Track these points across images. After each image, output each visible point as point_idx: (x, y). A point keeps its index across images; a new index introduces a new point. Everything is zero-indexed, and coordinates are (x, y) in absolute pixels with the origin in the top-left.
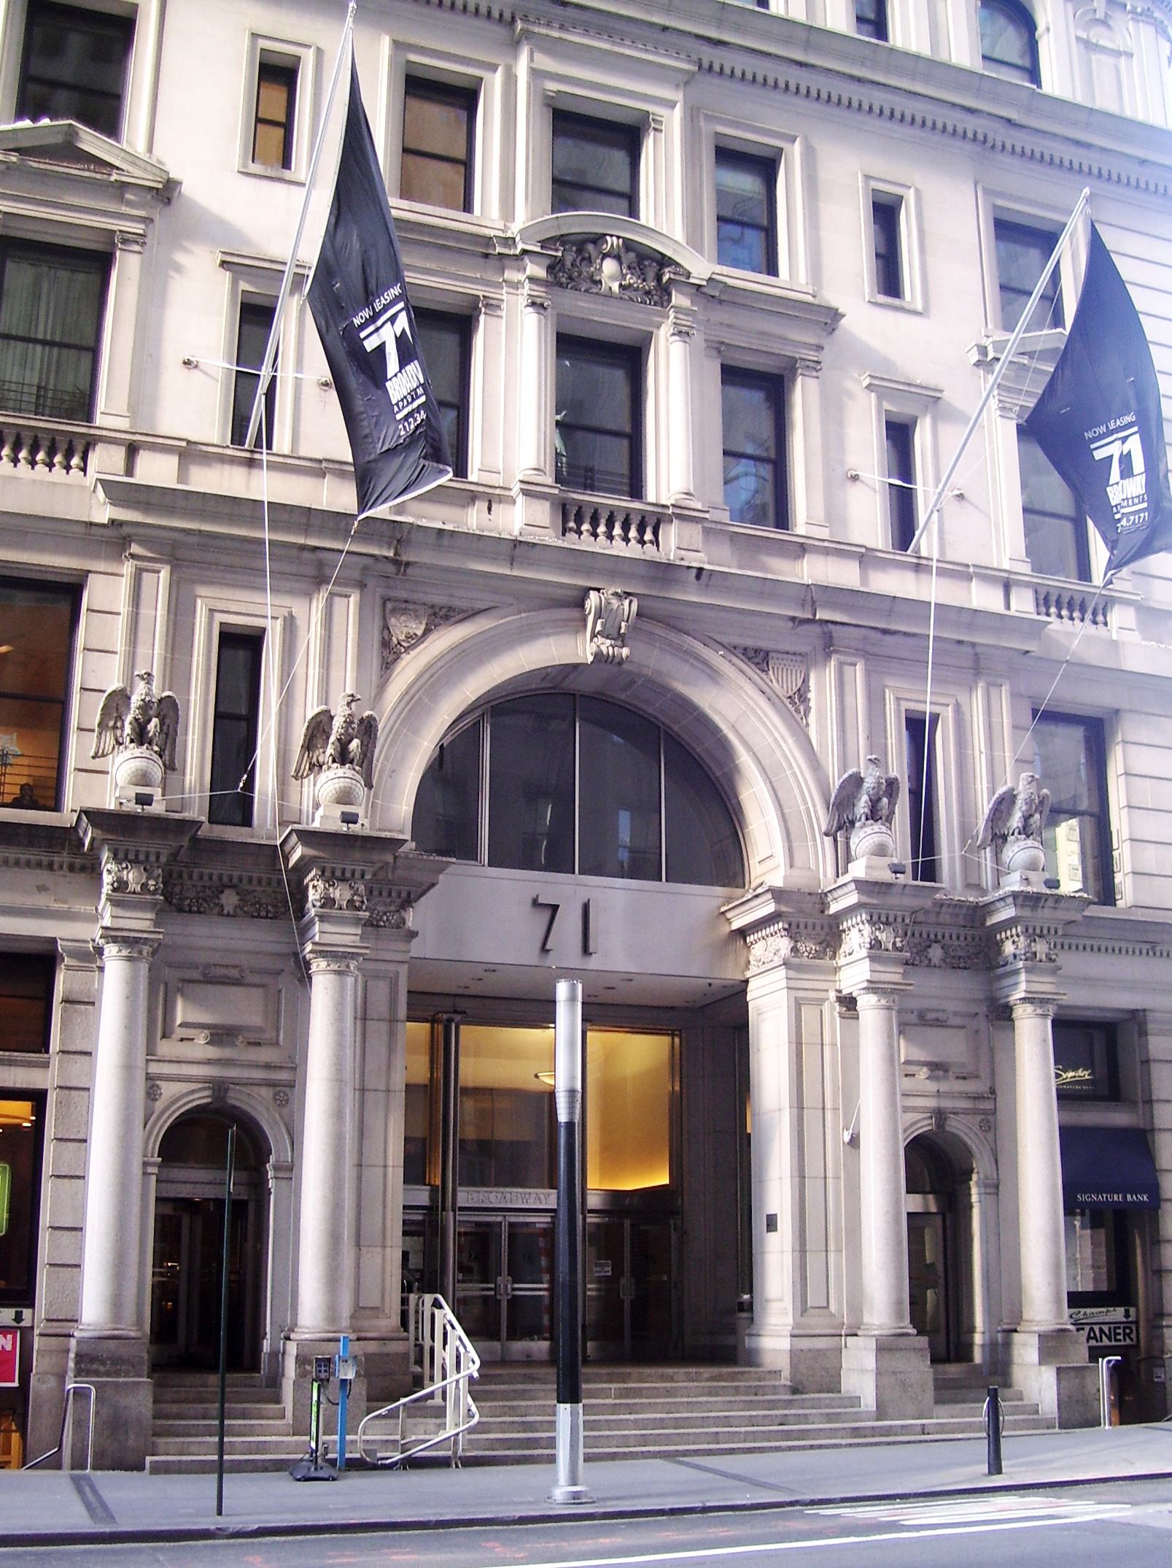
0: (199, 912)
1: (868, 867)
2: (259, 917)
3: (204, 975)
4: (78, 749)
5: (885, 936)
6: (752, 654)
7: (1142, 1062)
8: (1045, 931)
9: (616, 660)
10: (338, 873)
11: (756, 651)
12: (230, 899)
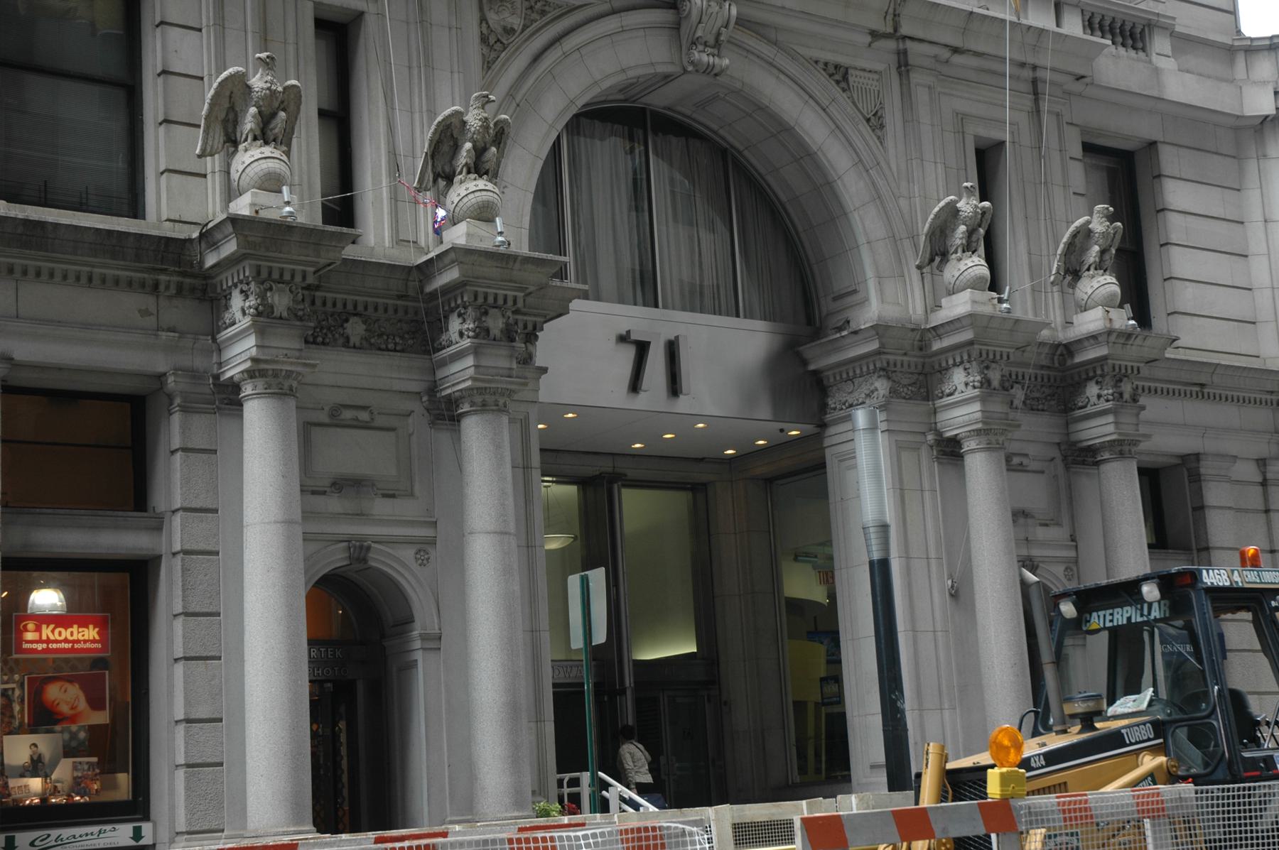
0: (323, 343)
1: (468, 235)
2: (388, 350)
3: (332, 416)
4: (159, 148)
5: (281, 301)
6: (832, 70)
7: (1194, 509)
8: (998, 357)
9: (715, 71)
10: (276, 276)
11: (836, 67)
12: (355, 329)
